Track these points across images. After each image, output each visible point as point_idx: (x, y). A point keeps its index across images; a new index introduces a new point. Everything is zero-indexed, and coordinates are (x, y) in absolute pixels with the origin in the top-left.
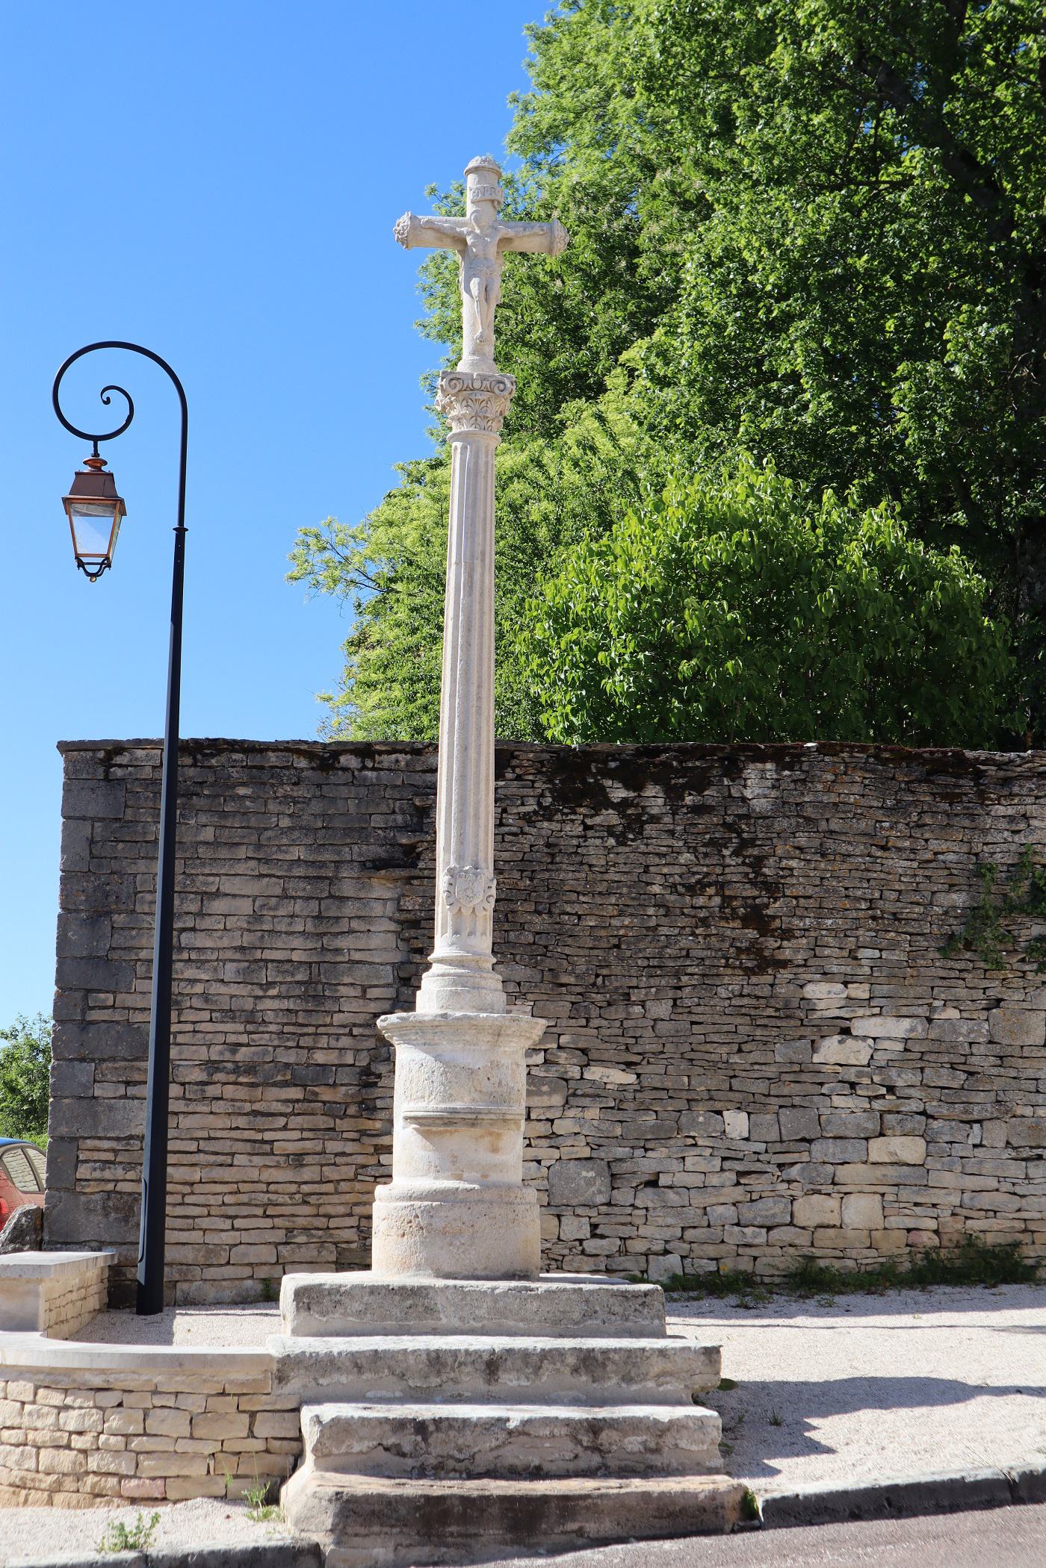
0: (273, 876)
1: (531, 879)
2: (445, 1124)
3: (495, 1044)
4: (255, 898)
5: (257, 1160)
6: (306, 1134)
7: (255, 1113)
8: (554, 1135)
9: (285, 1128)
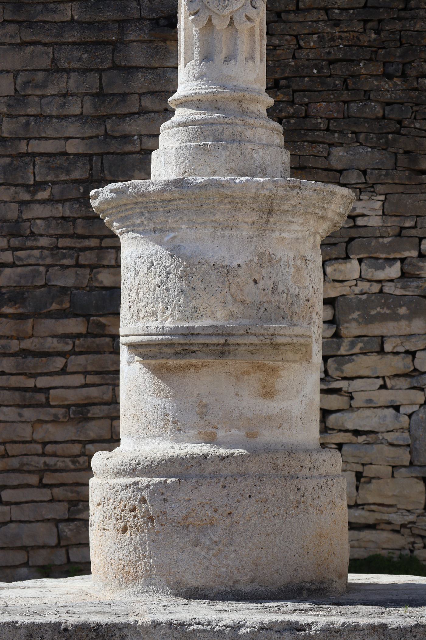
0: (39, 43)
1: (378, 32)
2: (179, 355)
3: (264, 228)
4: (16, 74)
5: (29, 414)
6: (90, 379)
7: (25, 353)
8: (416, 373)
9: (63, 371)
